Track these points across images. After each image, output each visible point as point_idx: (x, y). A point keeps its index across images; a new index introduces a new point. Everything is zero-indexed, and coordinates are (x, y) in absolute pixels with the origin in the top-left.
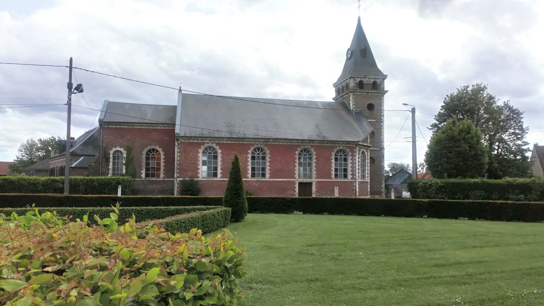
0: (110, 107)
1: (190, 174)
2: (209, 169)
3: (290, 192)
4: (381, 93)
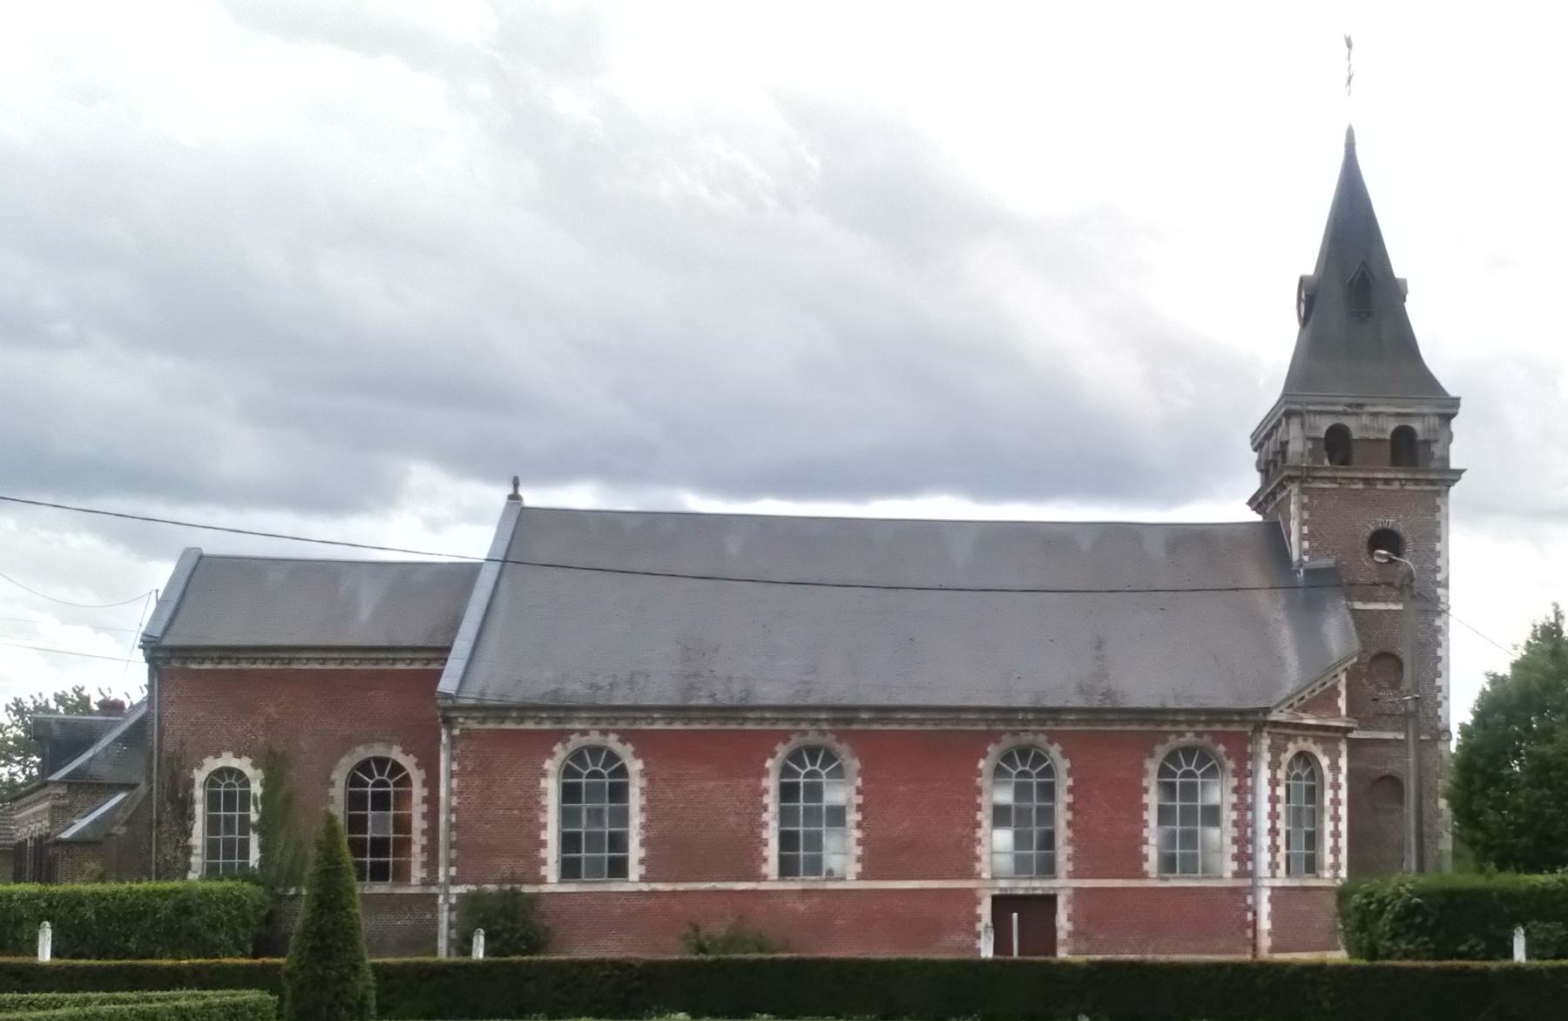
0: (203, 576)
1: (505, 865)
2: (1021, 841)
3: (959, 938)
4: (1431, 482)
